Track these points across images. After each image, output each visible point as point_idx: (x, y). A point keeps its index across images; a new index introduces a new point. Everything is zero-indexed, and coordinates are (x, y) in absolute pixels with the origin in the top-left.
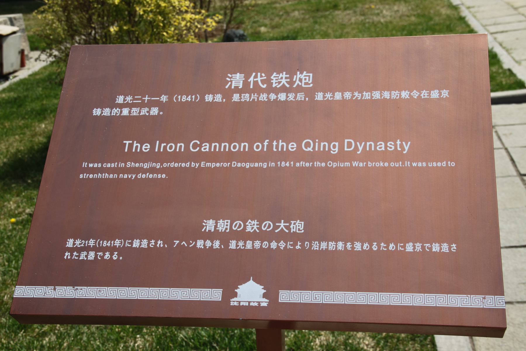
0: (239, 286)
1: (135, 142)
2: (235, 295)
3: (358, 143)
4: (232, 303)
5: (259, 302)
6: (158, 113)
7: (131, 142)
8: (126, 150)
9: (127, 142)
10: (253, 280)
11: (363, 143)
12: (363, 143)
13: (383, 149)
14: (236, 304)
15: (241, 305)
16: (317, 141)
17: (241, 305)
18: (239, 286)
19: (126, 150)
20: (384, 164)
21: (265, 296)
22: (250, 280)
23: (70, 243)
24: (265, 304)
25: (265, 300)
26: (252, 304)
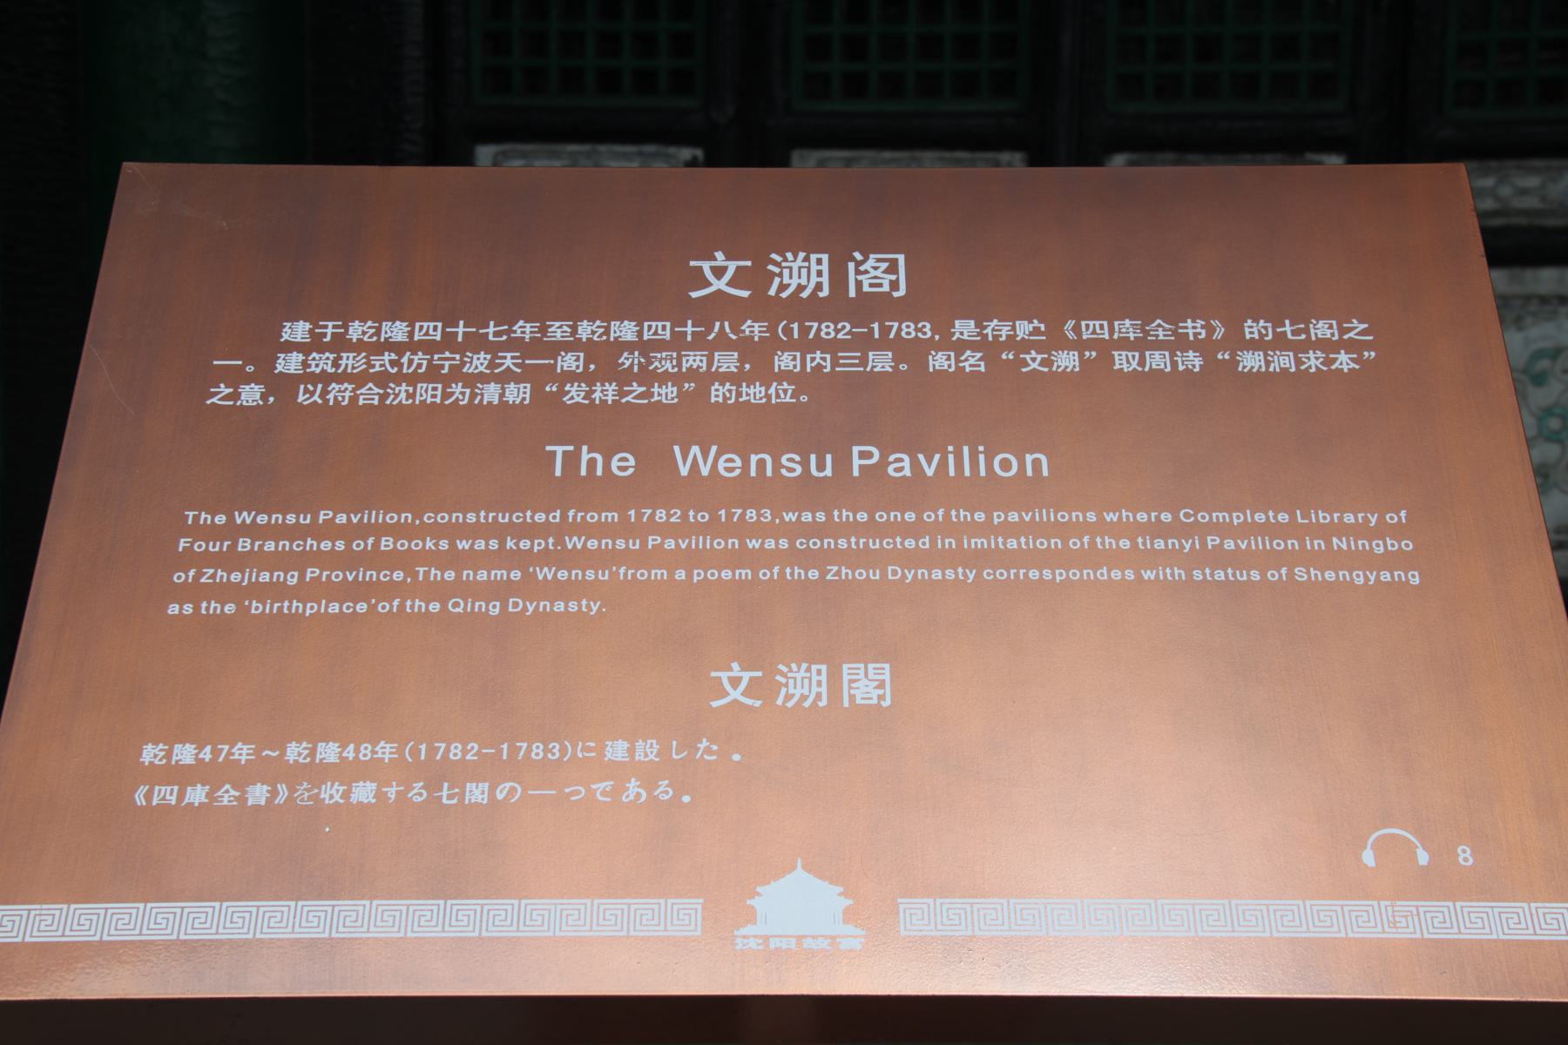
0: (758, 889)
1: (585, 448)
2: (751, 916)
3: (921, 457)
4: (739, 941)
5: (833, 938)
6: (895, 368)
7: (571, 448)
8: (558, 473)
9: (559, 450)
10: (804, 868)
11: (937, 457)
12: (937, 457)
13: (907, 472)
14: (752, 944)
15: (772, 946)
16: (950, 448)
17: (772, 946)
18: (758, 889)
19: (558, 473)
20: (517, 544)
21: (849, 916)
22: (794, 868)
23: (423, 747)
24: (856, 944)
25: (850, 929)
26: (808, 943)
